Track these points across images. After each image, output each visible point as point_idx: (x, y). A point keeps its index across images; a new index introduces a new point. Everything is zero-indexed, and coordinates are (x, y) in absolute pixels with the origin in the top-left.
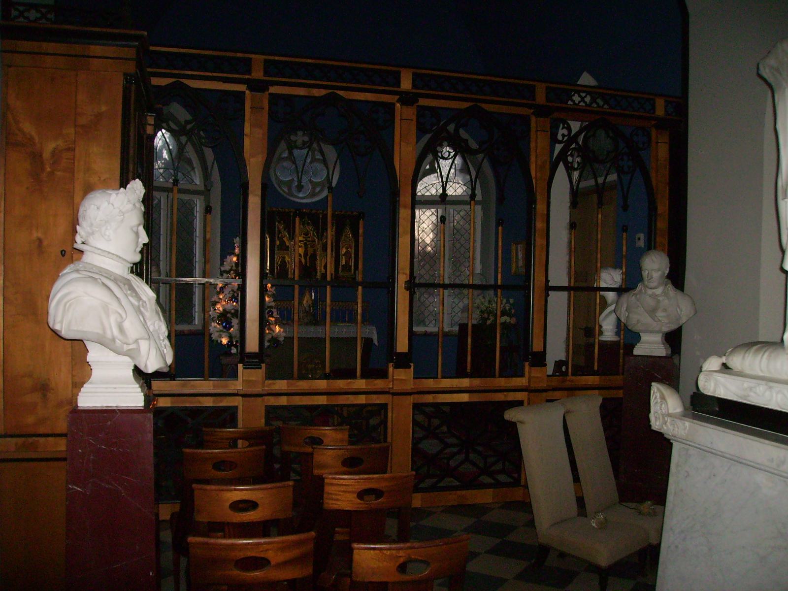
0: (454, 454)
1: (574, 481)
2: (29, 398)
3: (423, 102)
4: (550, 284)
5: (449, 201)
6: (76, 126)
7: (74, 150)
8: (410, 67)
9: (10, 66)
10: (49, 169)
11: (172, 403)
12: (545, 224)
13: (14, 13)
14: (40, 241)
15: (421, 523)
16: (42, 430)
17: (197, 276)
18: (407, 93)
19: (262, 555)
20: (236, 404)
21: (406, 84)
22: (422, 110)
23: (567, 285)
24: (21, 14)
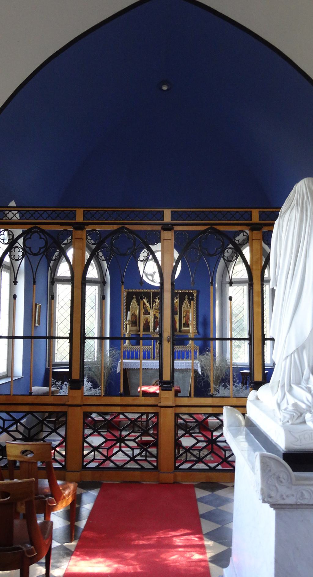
18: (167, 224)
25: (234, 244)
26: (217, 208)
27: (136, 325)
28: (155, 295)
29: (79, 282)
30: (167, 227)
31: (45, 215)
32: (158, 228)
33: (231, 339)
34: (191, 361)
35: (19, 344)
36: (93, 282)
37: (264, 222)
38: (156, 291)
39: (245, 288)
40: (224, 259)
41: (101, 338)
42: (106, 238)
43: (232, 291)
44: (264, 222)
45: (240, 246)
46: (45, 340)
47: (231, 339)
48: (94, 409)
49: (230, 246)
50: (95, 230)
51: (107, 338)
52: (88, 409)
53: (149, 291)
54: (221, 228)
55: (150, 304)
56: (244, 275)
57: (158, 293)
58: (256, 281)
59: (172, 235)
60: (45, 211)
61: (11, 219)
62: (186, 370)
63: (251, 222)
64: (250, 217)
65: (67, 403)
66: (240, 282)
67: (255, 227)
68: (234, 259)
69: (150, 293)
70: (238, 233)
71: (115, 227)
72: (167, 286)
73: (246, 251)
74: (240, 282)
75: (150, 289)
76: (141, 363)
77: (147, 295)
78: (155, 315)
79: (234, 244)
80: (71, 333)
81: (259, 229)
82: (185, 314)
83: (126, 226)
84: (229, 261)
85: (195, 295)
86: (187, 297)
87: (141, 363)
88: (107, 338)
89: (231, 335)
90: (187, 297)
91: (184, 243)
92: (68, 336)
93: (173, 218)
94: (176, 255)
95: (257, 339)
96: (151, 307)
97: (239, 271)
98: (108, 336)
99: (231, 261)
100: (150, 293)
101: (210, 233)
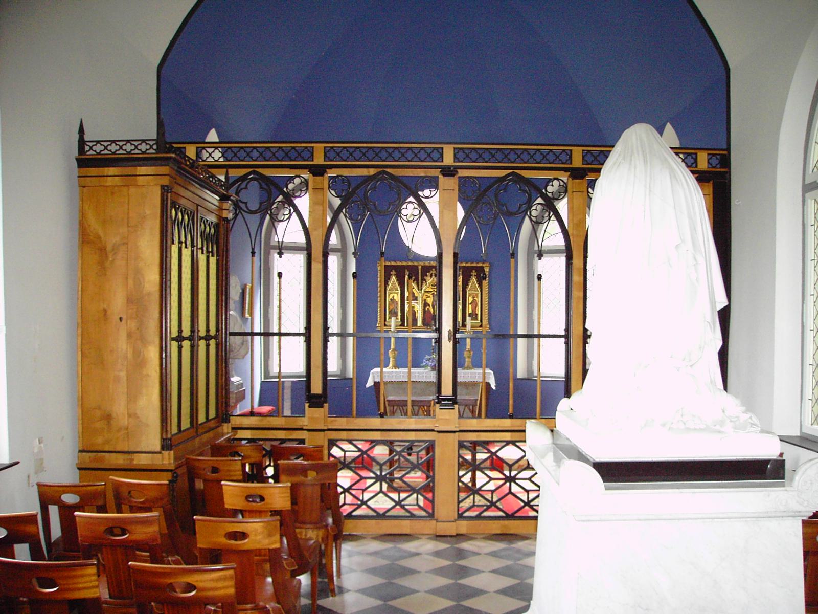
0: (468, 509)
1: (532, 588)
2: (99, 425)
3: (462, 173)
4: (563, 340)
5: (342, 245)
6: (128, 226)
7: (127, 244)
8: (450, 143)
9: (84, 187)
10: (111, 259)
11: (251, 435)
12: (582, 278)
13: (87, 148)
14: (105, 311)
15: (452, 563)
16: (106, 449)
17: (410, 341)
18: (449, 167)
19: (194, 583)
20: (303, 438)
21: (449, 159)
22: (464, 181)
23: (541, 339)
24: (91, 148)
25: (544, 197)
26: (468, 144)
27: (477, 319)
28: (426, 270)
29: (315, 254)
30: (448, 172)
31: (357, 154)
32: (436, 173)
33: (280, 334)
34: (406, 370)
35: (350, 341)
36: (335, 250)
37: (590, 166)
38: (427, 263)
39: (562, 260)
40: (531, 220)
41: (342, 335)
42: (358, 187)
43: (279, 263)
44: (590, 166)
45: (552, 201)
46: (259, 337)
47: (280, 334)
48: (344, 435)
49: (540, 200)
50: (341, 176)
51: (350, 335)
52: (334, 435)
53: (416, 264)
54: (527, 174)
55: (418, 284)
56: (560, 242)
57: (434, 268)
58: (575, 251)
59: (455, 183)
60: (242, 148)
61: (217, 161)
62: (474, 384)
63: (571, 166)
64: (326, 152)
65: (436, 429)
66: (554, 251)
67: (577, 174)
68: (545, 219)
69: (417, 267)
70: (548, 182)
71: (372, 172)
72: (448, 260)
73: (562, 206)
74: (554, 251)
75: (417, 261)
76: (409, 372)
77: (413, 271)
78: (425, 300)
79: (544, 197)
80: (567, 330)
81: (582, 177)
82: (471, 299)
83: (388, 170)
84: (536, 223)
85: (487, 270)
86: (474, 273)
87: (409, 372)
88: (350, 335)
89: (539, 330)
90: (474, 273)
91: (474, 196)
92: (563, 333)
93: (456, 158)
94: (461, 213)
95: (577, 338)
96: (420, 289)
97: (551, 235)
98: (351, 331)
99: (541, 223)
100: (417, 267)
101: (510, 180)
